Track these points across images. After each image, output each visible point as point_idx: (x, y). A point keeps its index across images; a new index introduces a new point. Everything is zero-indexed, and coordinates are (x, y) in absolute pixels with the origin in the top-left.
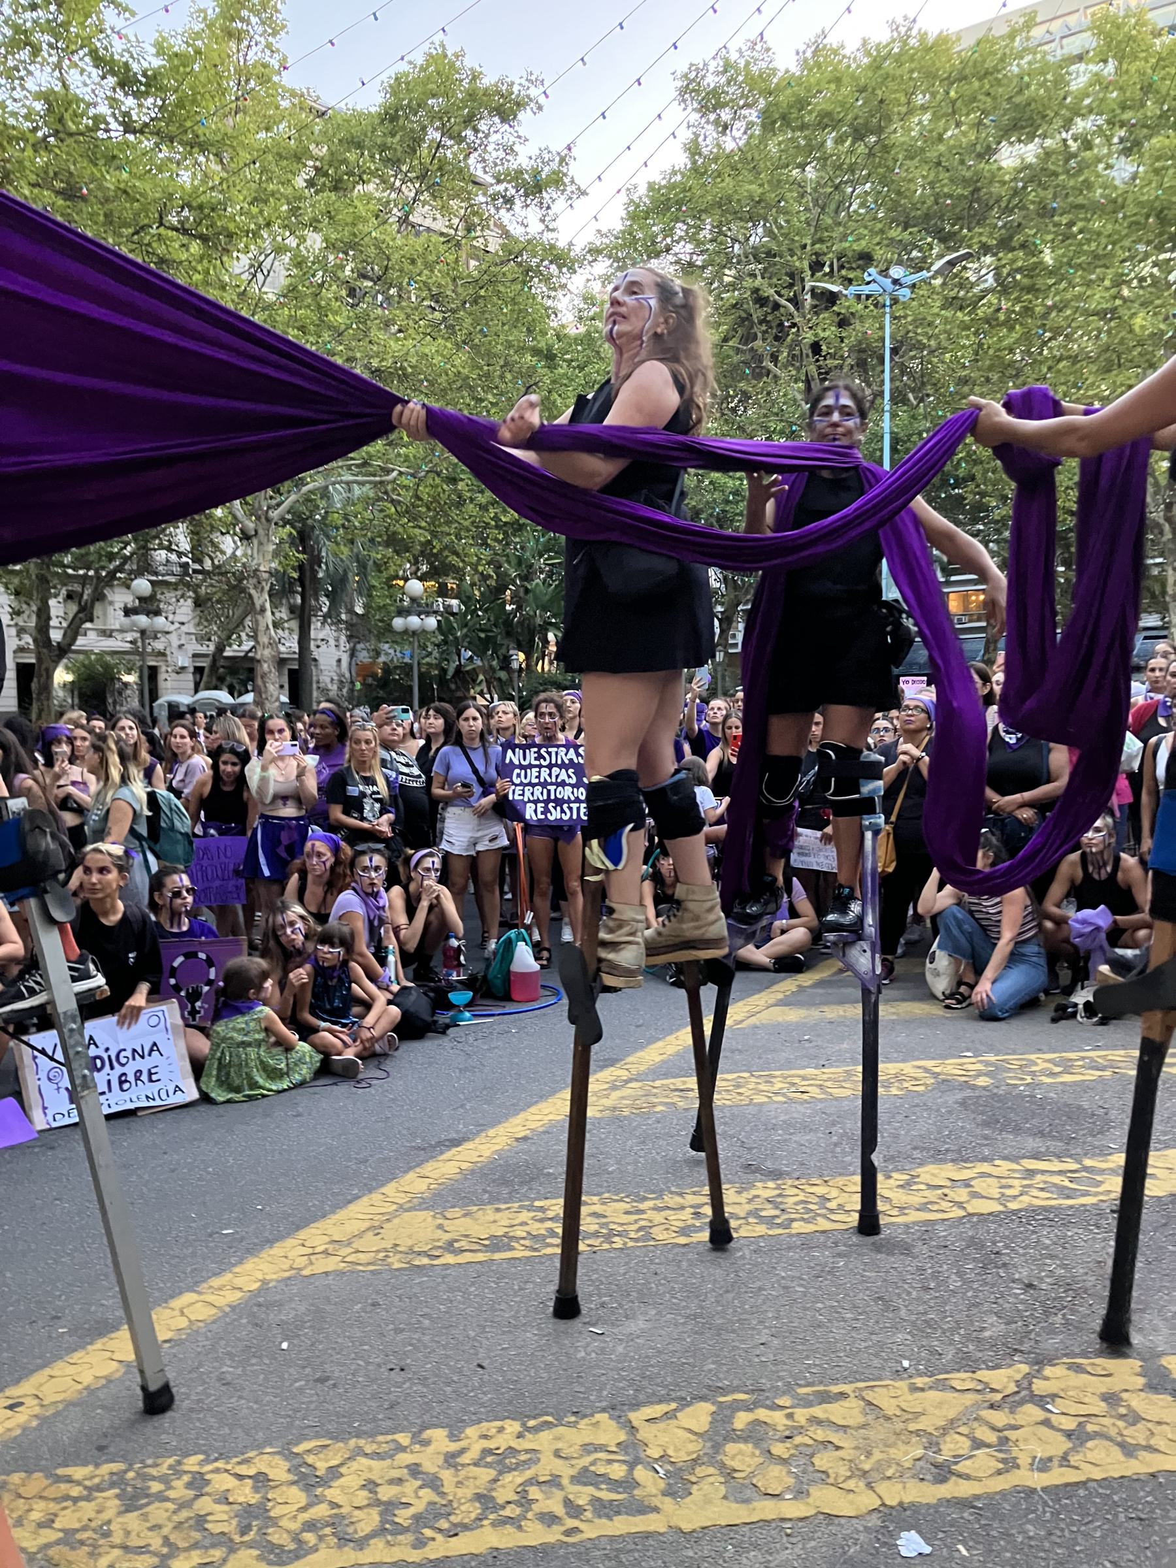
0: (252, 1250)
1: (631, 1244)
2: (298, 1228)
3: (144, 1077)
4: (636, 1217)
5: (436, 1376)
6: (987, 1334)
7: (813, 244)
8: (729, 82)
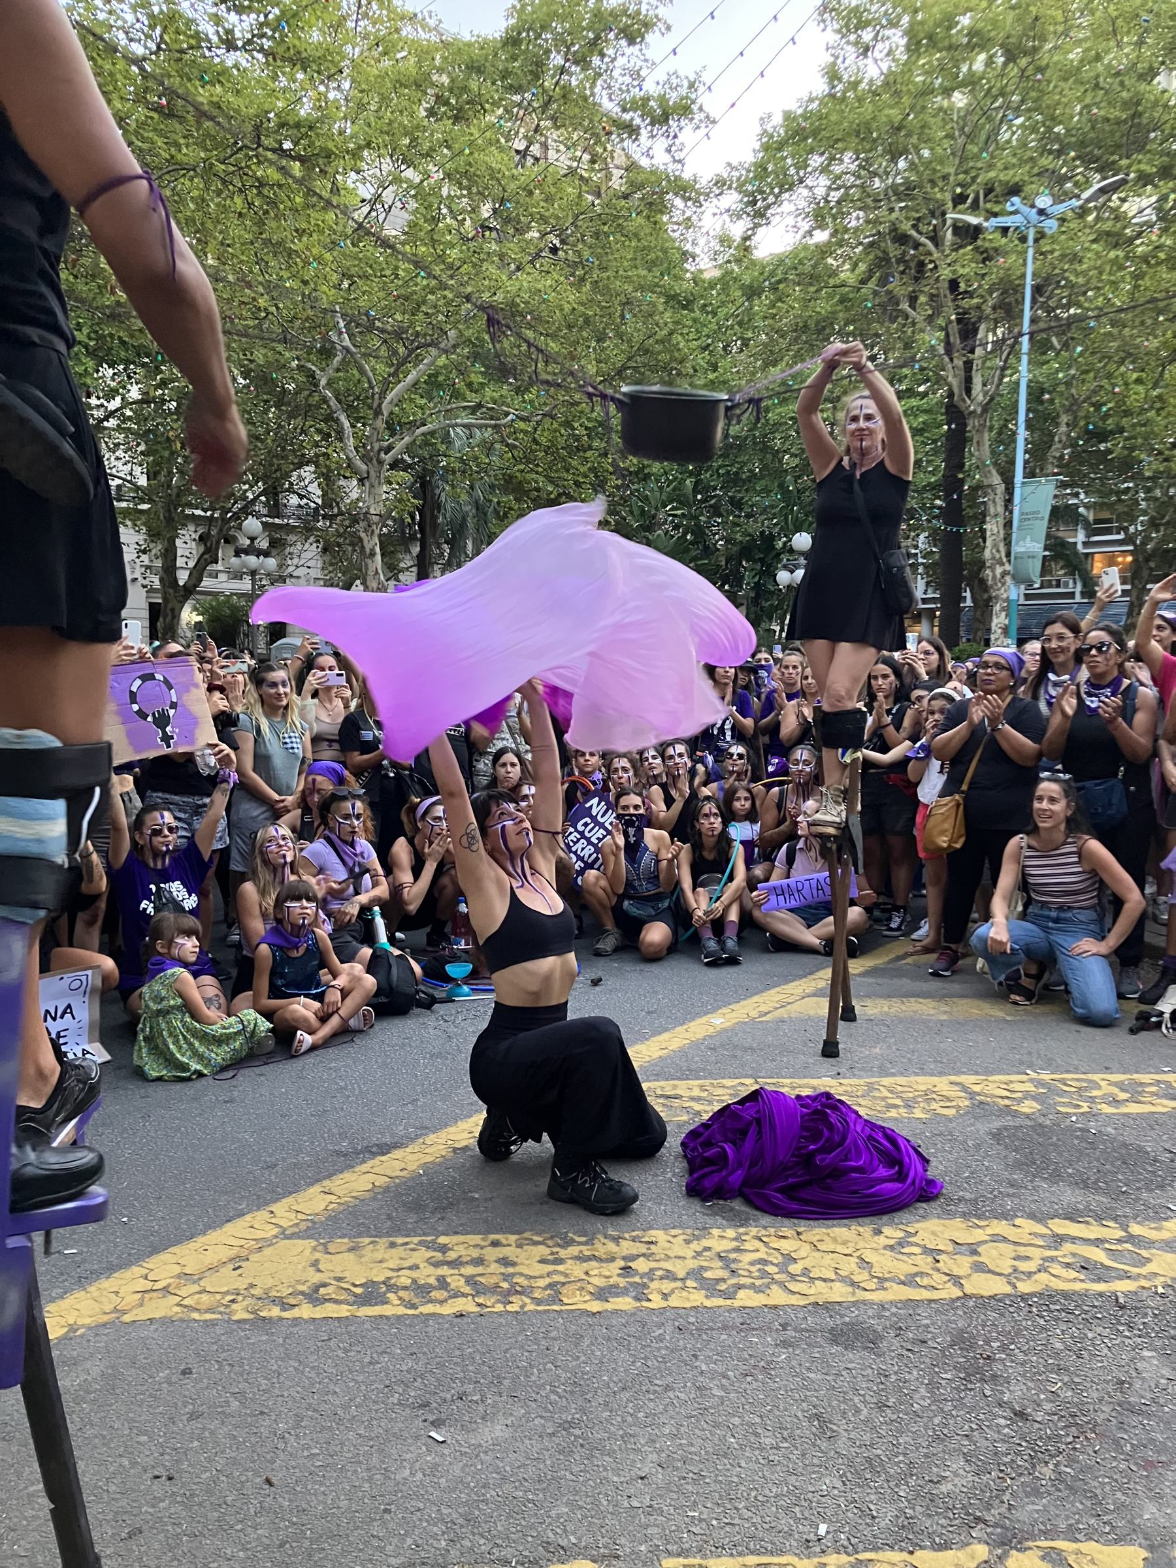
0: (82, 1281)
1: (531, 1307)
2: (155, 1250)
4: (551, 1268)
5: (209, 1492)
6: (944, 1488)
7: (957, 174)
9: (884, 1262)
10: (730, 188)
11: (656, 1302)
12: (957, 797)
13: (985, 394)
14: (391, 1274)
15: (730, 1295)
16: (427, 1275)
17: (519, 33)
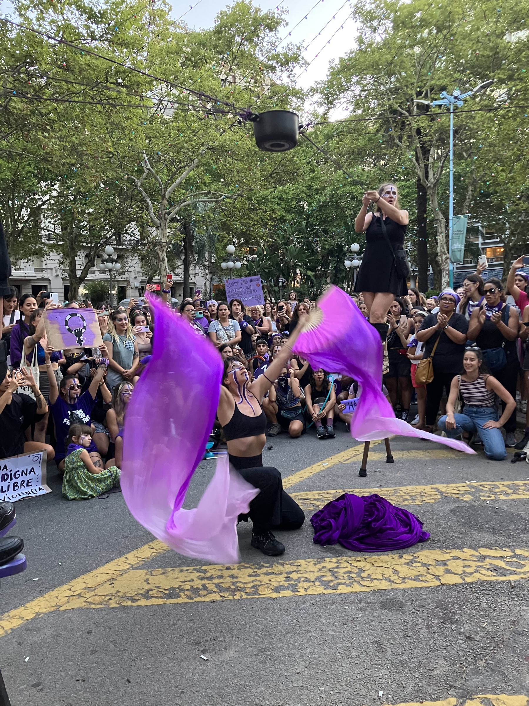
0: (41, 593)
1: (245, 596)
2: (74, 577)
3: (25, 484)
4: (254, 578)
6: (435, 673)
8: (376, 7)
9: (404, 571)
10: (317, 92)
11: (302, 592)
12: (429, 359)
13: (435, 179)
14: (181, 584)
15: (335, 588)
16: (198, 584)
17: (221, 28)
